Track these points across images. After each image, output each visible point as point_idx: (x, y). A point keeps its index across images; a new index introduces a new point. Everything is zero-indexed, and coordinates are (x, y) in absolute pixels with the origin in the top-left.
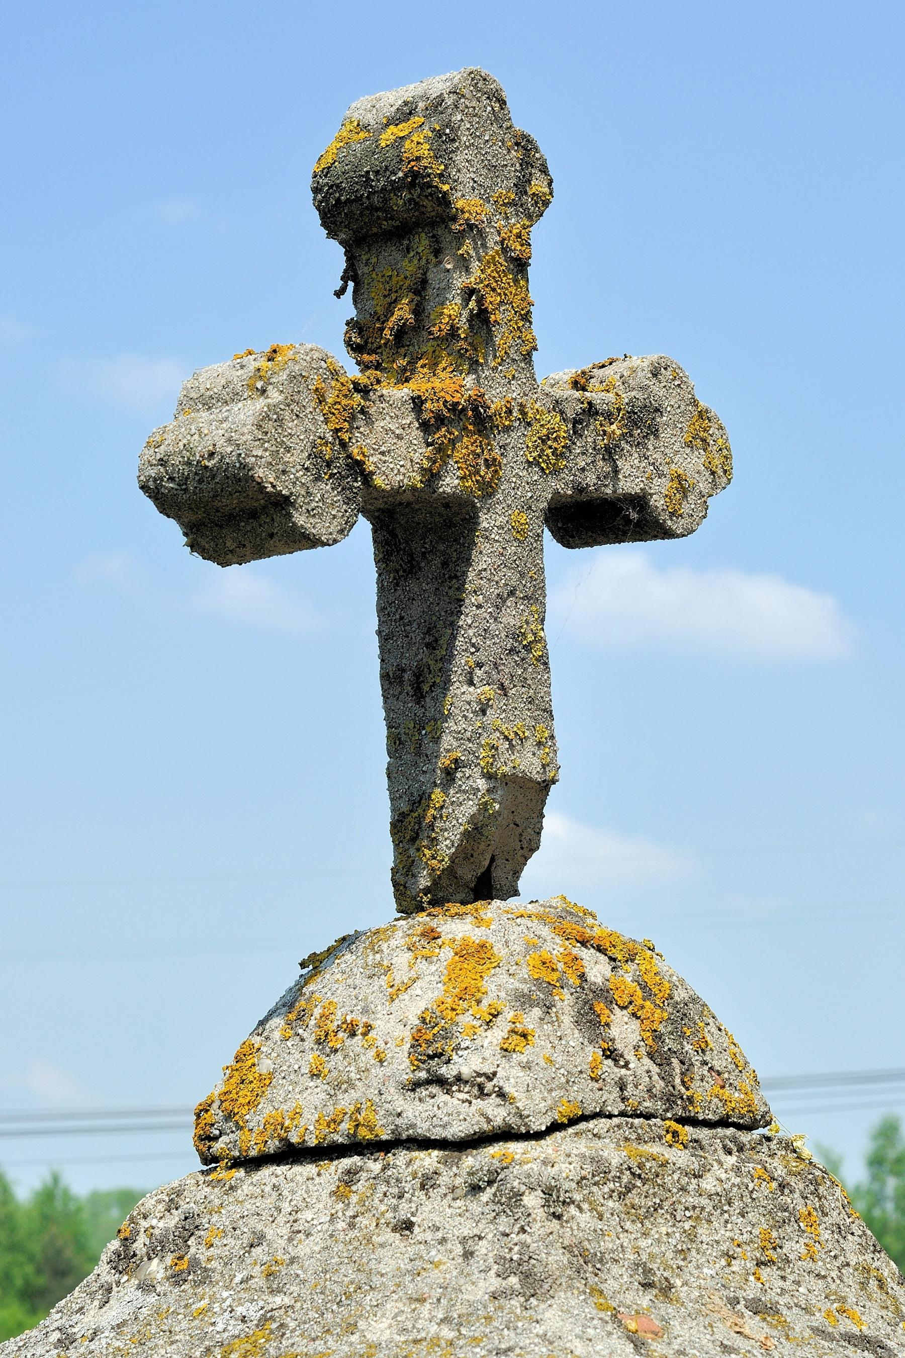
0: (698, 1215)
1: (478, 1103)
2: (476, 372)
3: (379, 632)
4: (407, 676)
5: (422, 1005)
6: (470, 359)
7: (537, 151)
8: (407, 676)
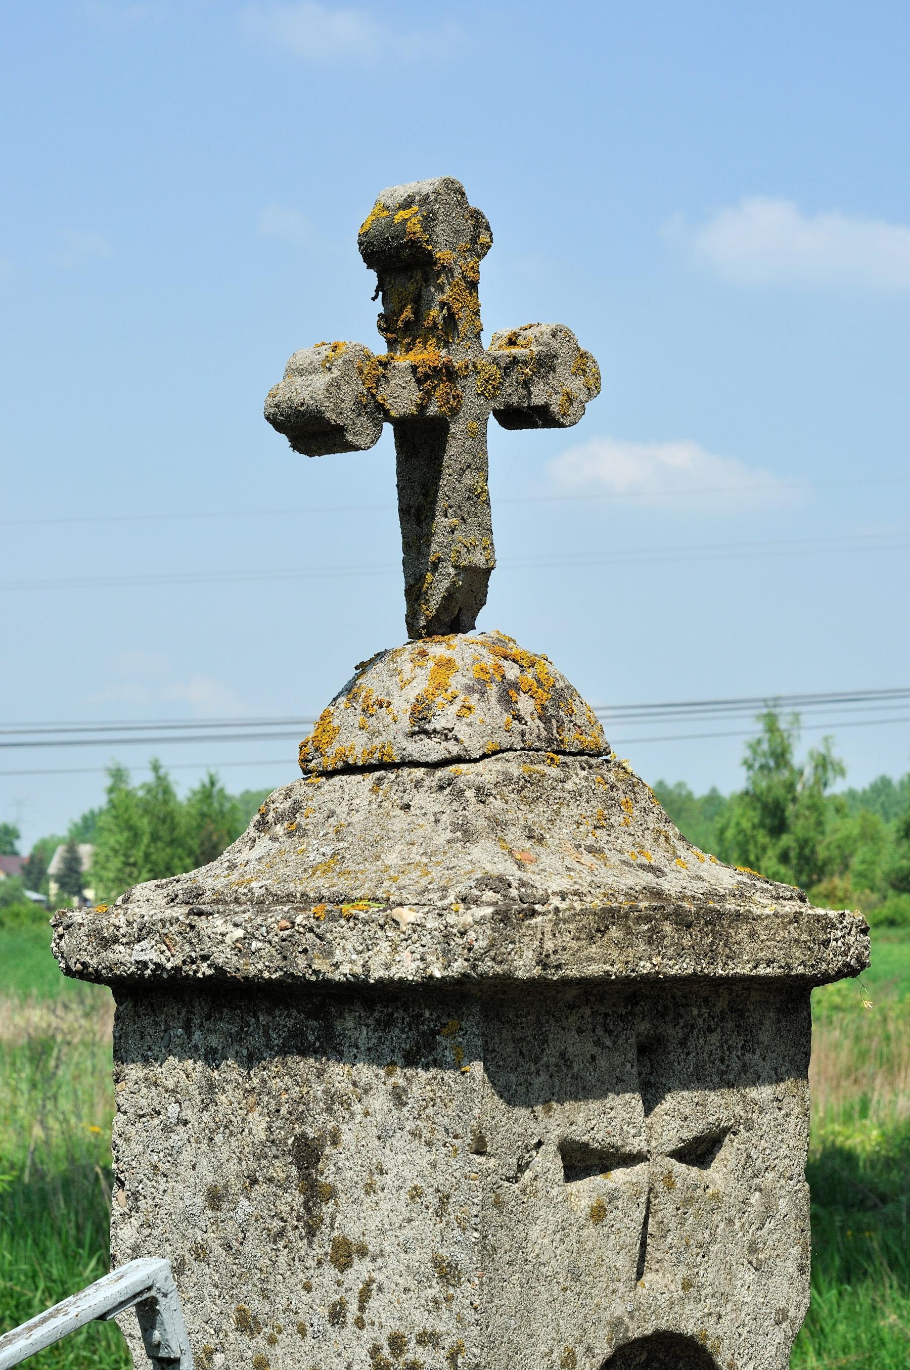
0: (561, 801)
1: (444, 744)
2: (448, 347)
3: (397, 486)
4: (413, 510)
5: (417, 692)
6: (444, 340)
7: (483, 217)
8: (413, 510)
